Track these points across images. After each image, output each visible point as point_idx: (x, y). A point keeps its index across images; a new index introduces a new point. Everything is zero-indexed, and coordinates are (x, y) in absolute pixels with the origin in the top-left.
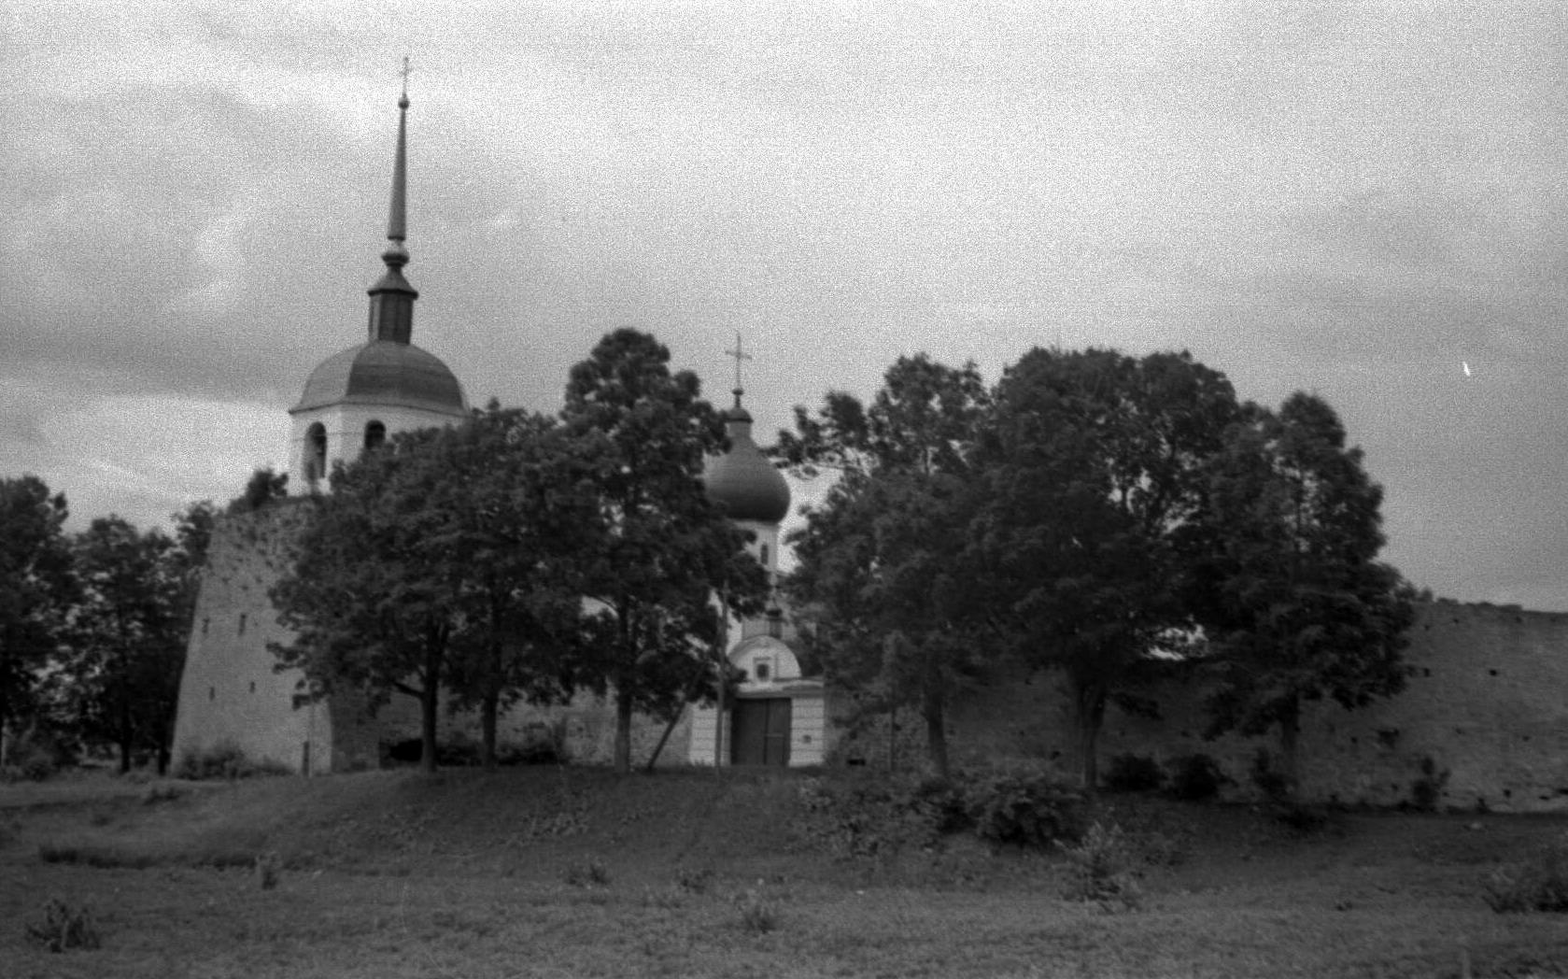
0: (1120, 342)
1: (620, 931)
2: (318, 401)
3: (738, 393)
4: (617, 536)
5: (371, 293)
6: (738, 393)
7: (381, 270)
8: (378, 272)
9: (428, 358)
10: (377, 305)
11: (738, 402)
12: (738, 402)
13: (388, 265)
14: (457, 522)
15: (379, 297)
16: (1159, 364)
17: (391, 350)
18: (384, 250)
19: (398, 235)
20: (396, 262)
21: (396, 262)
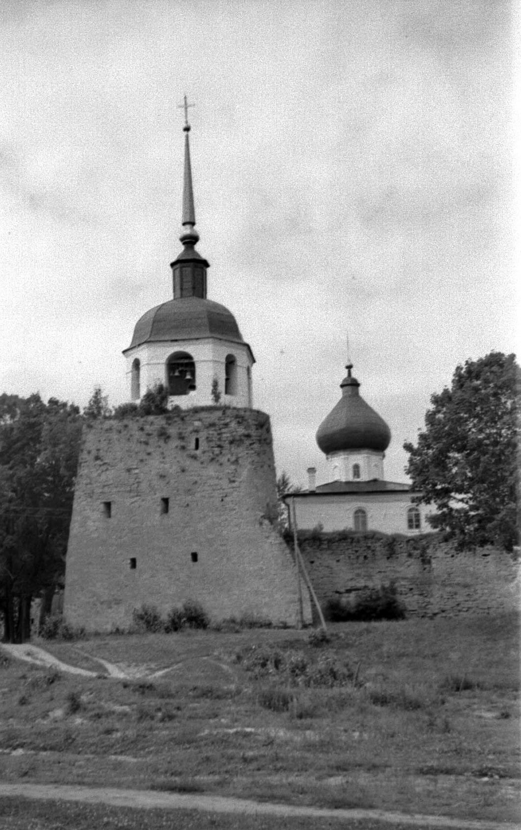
0: (29, 392)
1: (42, 622)
2: (152, 339)
3: (349, 367)
4: (449, 533)
5: (173, 265)
6: (349, 367)
7: (180, 248)
8: (178, 250)
9: (216, 306)
10: (177, 272)
11: (349, 374)
12: (349, 374)
13: (184, 244)
14: (453, 520)
15: (178, 266)
16: (12, 397)
17: (192, 305)
18: (180, 235)
19: (190, 222)
20: (190, 241)
21: (190, 241)
